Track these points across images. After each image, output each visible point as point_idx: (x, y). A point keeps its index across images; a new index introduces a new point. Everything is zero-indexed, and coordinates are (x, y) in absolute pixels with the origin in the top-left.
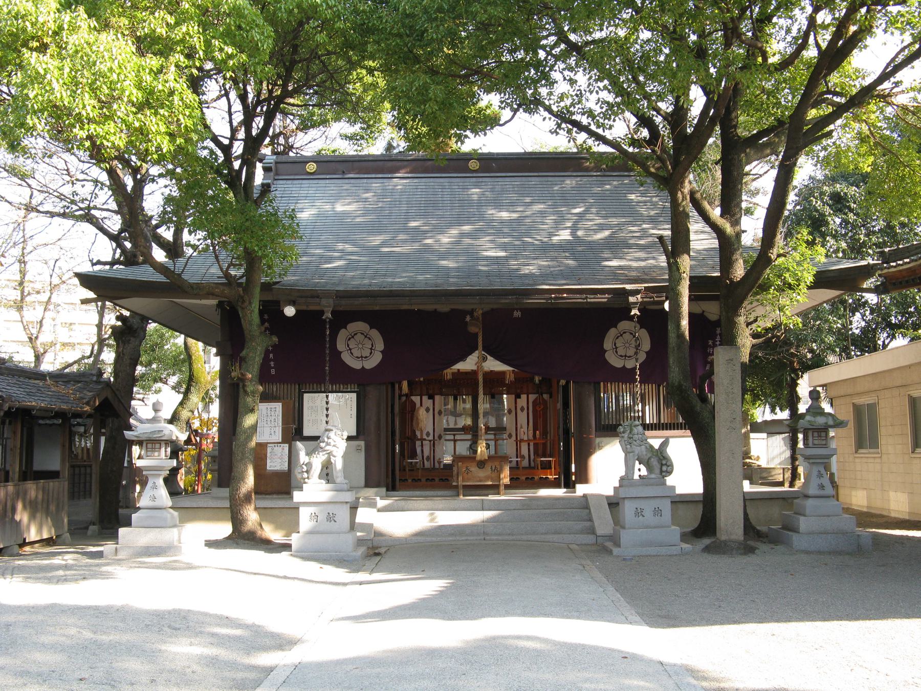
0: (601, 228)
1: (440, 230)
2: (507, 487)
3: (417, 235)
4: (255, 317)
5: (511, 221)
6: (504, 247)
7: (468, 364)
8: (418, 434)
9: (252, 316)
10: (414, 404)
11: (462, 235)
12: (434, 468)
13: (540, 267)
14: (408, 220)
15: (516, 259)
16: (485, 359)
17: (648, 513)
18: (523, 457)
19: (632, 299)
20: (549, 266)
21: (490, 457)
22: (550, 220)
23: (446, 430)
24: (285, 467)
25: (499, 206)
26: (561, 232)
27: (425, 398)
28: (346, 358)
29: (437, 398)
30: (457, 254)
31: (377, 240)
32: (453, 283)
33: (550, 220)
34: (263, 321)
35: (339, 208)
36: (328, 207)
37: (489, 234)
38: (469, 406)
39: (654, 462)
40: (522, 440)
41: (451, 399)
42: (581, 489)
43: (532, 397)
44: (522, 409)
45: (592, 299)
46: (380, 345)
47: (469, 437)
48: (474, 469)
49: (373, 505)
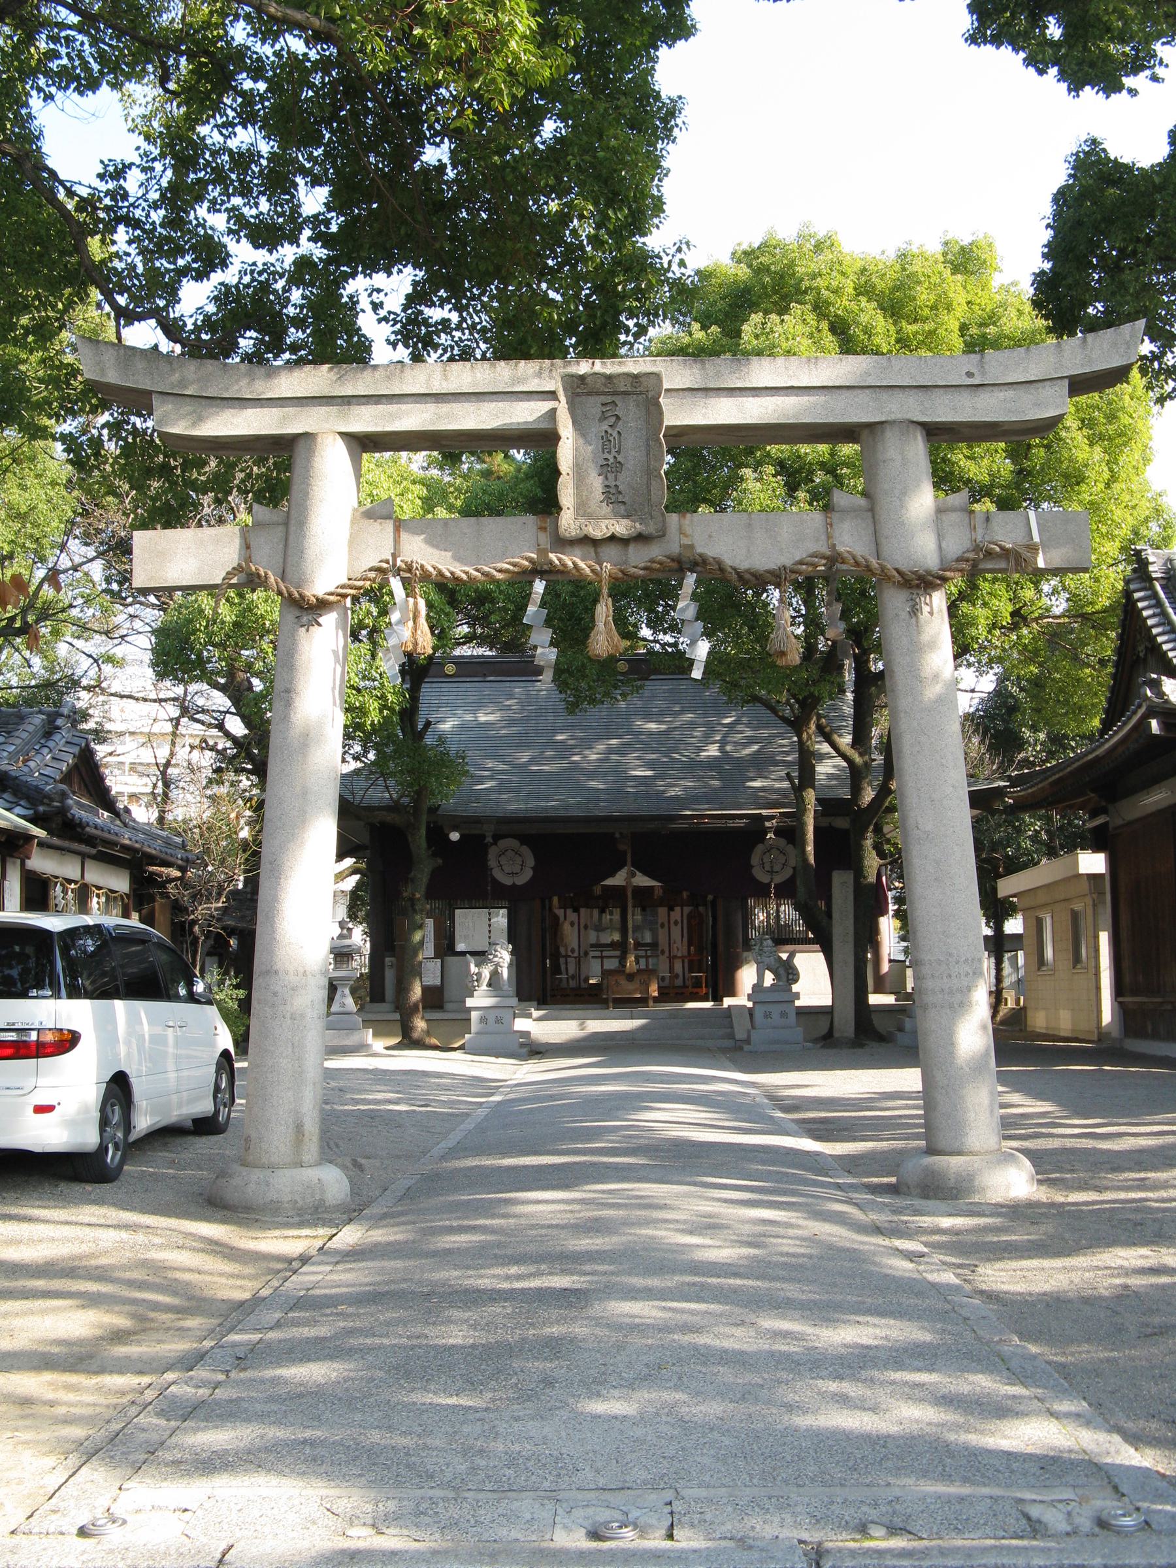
0: (751, 741)
1: (587, 744)
2: (656, 1000)
3: (564, 750)
4: (424, 844)
5: (660, 733)
6: (650, 765)
7: (618, 879)
8: (562, 950)
9: (419, 841)
10: (556, 918)
11: (610, 751)
12: (579, 988)
13: (686, 788)
14: (555, 733)
15: (663, 779)
16: (634, 875)
17: (775, 1016)
18: (677, 976)
19: (767, 824)
20: (694, 788)
21: (639, 971)
22: (699, 732)
23: (592, 946)
24: (438, 982)
25: (648, 717)
26: (711, 747)
27: (569, 911)
28: (498, 875)
29: (583, 910)
30: (606, 774)
31: (524, 757)
32: (603, 808)
33: (699, 732)
34: (429, 847)
35: (483, 718)
36: (469, 717)
37: (638, 750)
38: (617, 916)
39: (782, 971)
40: (675, 957)
41: (596, 912)
42: (728, 1002)
43: (687, 910)
44: (676, 923)
45: (731, 824)
46: (531, 862)
47: (618, 953)
48: (623, 982)
49: (529, 1016)
